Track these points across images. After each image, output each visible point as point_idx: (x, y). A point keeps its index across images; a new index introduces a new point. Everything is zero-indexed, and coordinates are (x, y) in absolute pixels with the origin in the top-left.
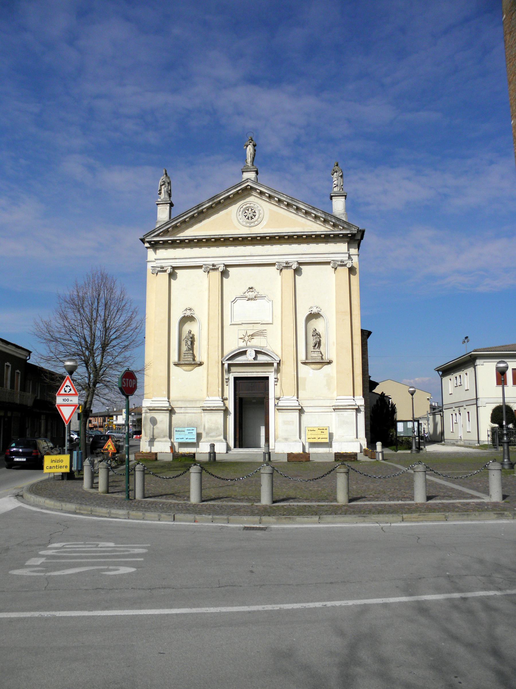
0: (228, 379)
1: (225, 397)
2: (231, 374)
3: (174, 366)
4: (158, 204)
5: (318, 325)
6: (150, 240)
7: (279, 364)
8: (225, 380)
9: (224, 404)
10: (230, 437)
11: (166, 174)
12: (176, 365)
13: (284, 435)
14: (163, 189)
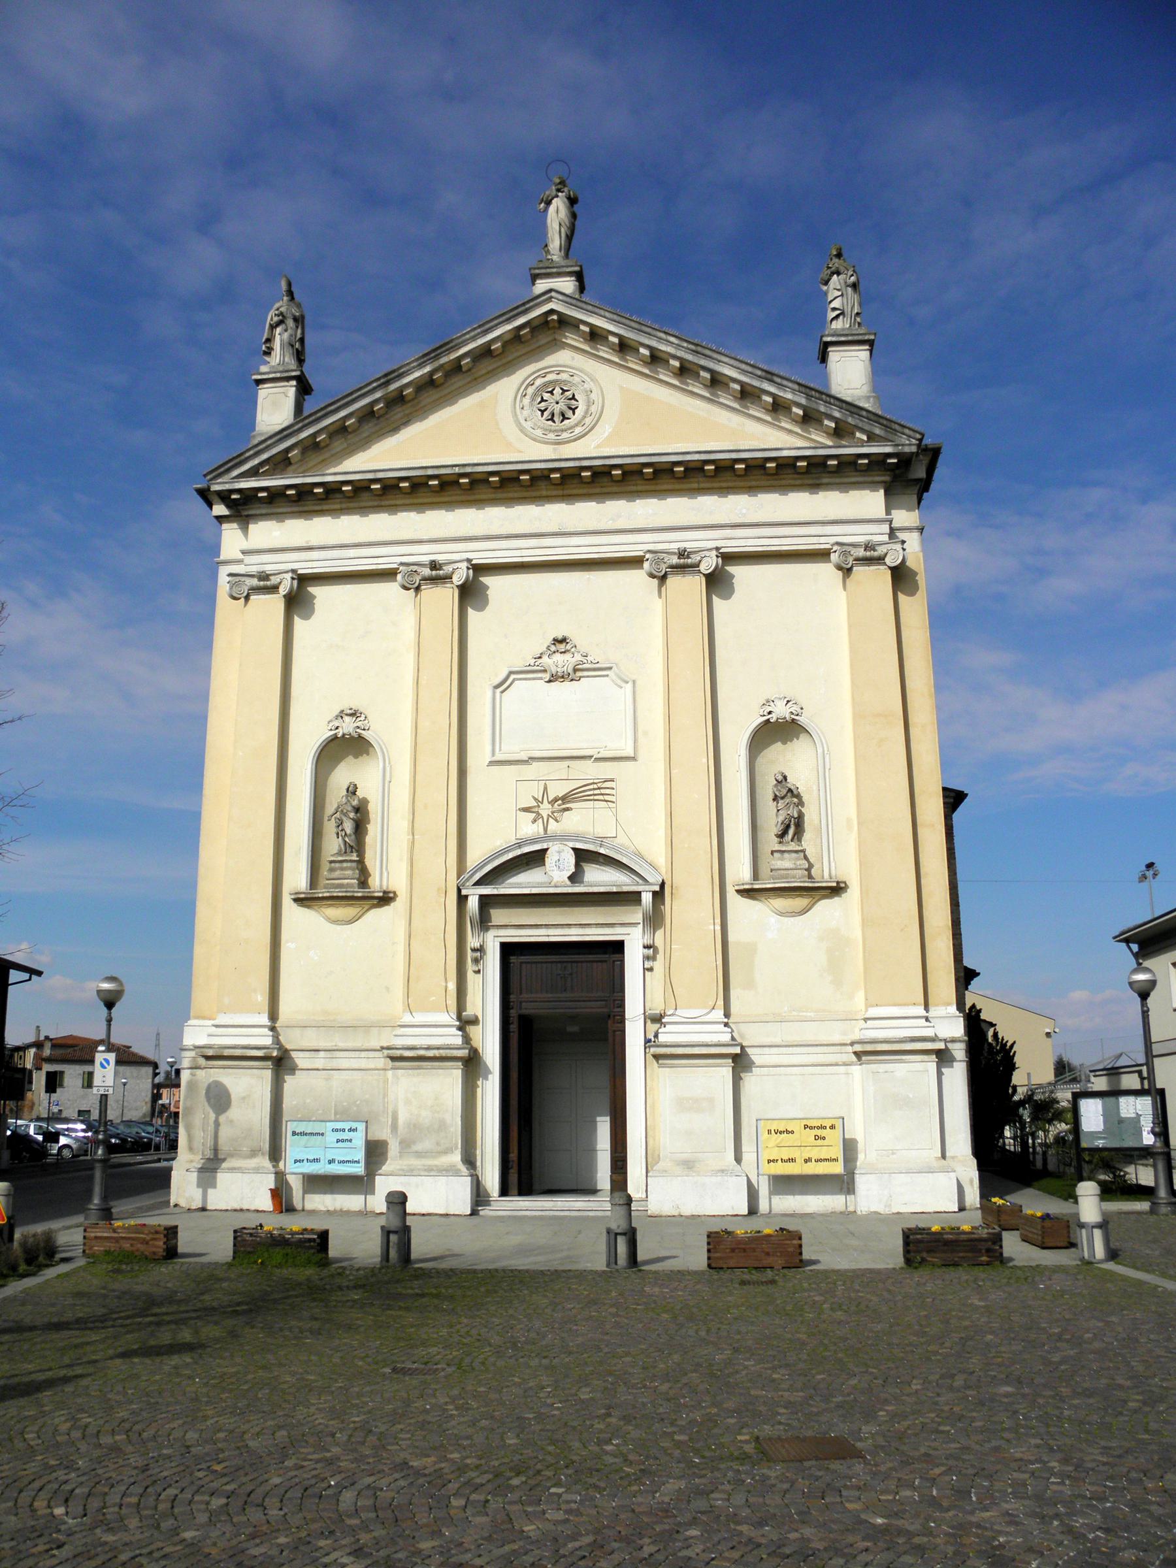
0: (481, 950)
1: (469, 1012)
2: (491, 934)
3: (294, 905)
4: (258, 382)
5: (794, 762)
6: (227, 487)
7: (658, 896)
8: (469, 954)
9: (467, 1039)
10: (488, 1157)
11: (290, 293)
12: (300, 901)
13: (682, 1156)
14: (278, 338)
